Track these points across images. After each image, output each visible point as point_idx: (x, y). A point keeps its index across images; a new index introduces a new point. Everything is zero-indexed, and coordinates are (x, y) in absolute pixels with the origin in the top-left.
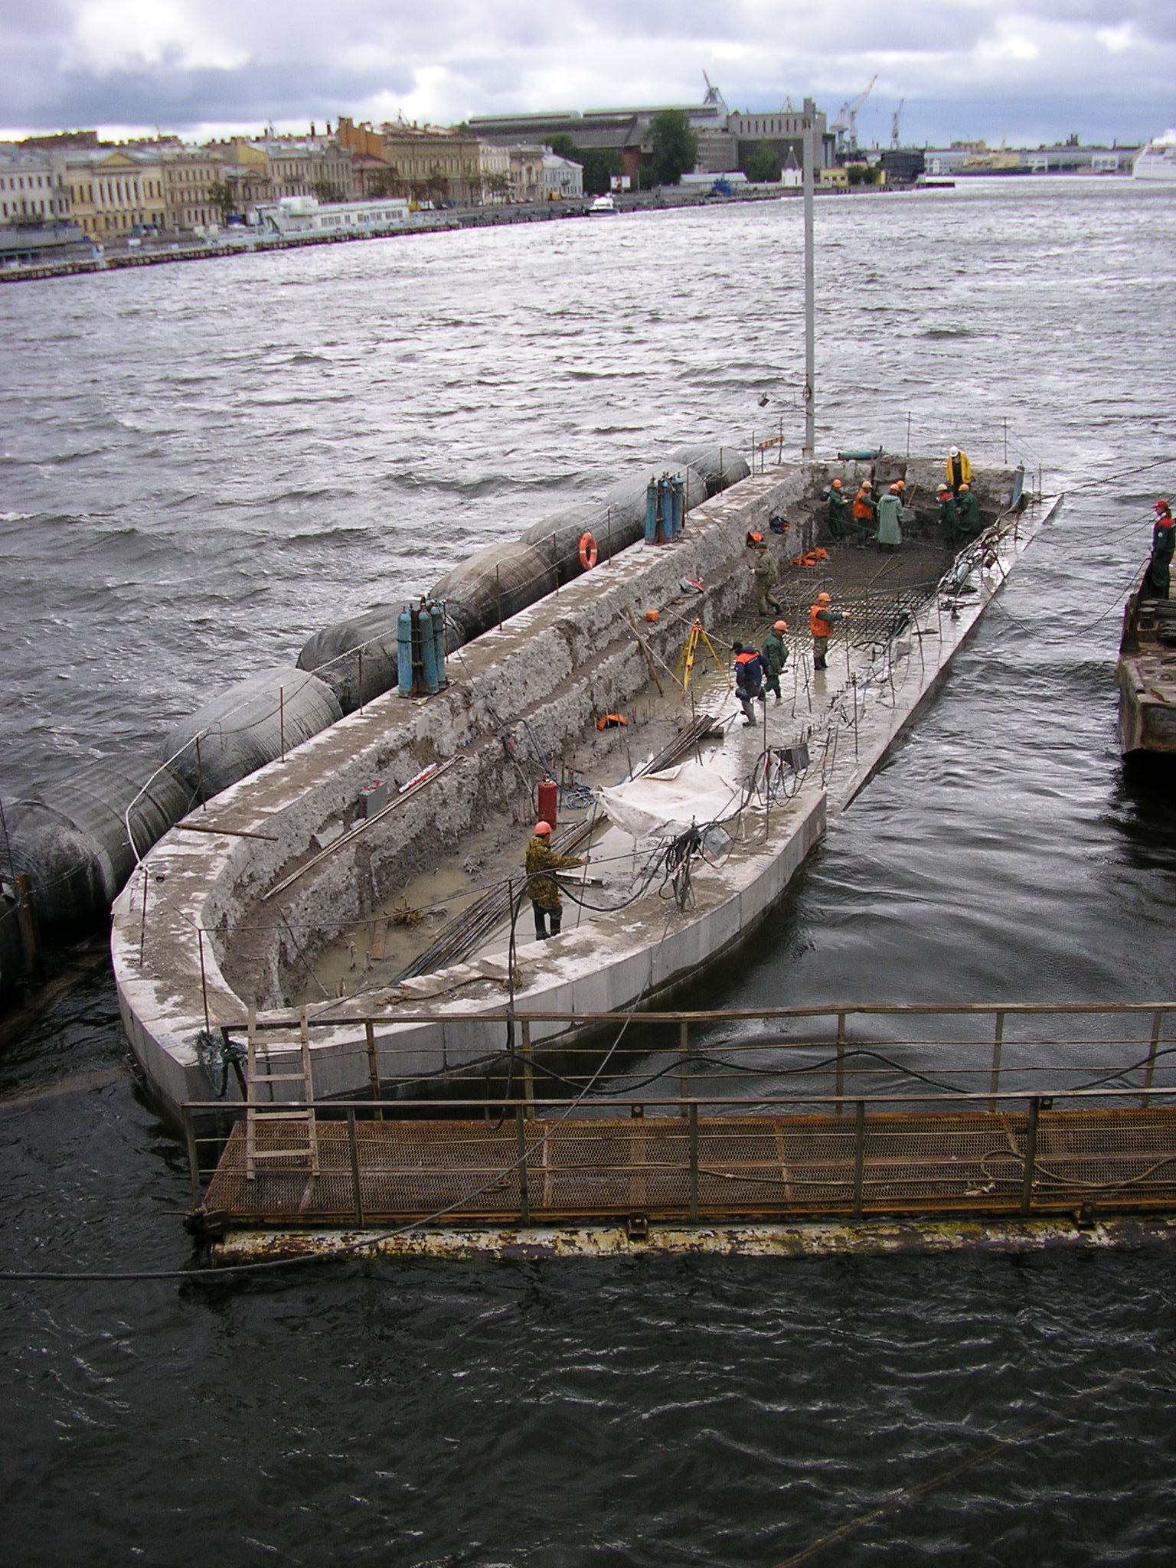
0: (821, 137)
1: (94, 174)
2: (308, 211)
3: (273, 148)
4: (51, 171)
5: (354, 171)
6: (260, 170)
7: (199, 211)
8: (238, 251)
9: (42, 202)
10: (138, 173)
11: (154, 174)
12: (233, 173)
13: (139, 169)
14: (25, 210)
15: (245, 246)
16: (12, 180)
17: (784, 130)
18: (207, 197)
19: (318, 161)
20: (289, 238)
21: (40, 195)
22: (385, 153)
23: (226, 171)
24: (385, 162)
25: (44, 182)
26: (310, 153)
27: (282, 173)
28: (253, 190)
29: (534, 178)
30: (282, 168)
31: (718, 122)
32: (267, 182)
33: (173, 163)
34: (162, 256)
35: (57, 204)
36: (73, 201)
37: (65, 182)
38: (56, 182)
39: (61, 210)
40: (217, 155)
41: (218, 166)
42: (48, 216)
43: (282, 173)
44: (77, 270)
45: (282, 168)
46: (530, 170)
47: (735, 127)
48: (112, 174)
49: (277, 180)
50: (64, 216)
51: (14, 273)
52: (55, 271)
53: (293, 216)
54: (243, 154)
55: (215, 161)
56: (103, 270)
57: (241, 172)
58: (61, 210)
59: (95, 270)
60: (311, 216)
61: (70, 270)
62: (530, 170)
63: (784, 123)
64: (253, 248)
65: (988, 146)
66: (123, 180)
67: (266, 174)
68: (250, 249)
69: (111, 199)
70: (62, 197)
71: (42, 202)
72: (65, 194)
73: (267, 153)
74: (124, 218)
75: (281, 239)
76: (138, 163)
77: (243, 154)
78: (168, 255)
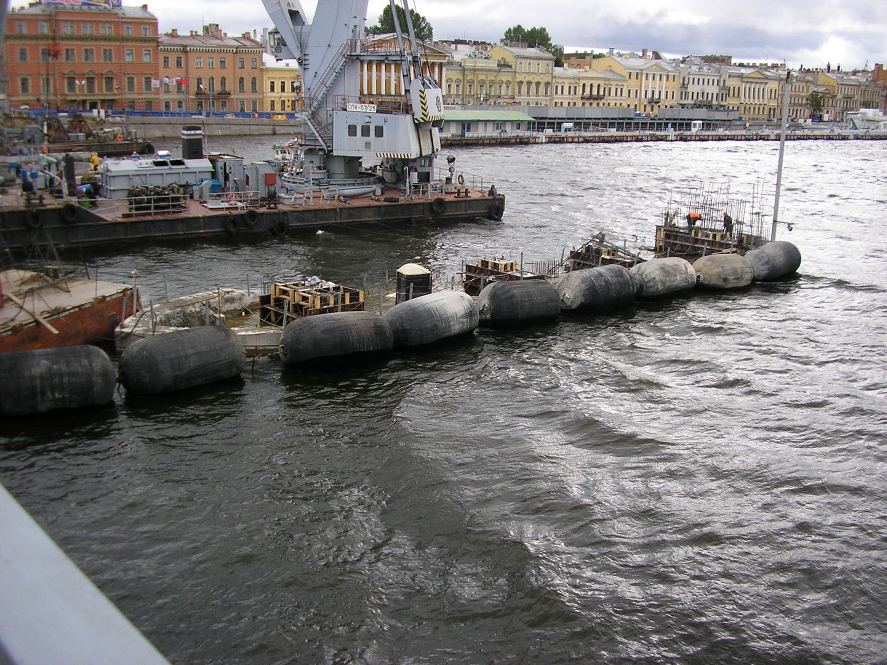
1: (742, 82)
2: (877, 118)
3: (839, 78)
4: (721, 77)
5: (882, 96)
6: (831, 89)
7: (795, 109)
8: (844, 138)
9: (693, 93)
10: (766, 83)
11: (774, 85)
12: (815, 89)
13: (767, 81)
15: (848, 136)
16: (699, 79)
18: (804, 102)
19: (863, 88)
20: (872, 134)
21: (713, 90)
23: (812, 88)
25: (716, 83)
26: (860, 83)
27: (843, 93)
28: (826, 100)
30: (843, 89)
32: (834, 97)
34: (595, 137)
35: (720, 96)
38: (722, 84)
39: (722, 100)
40: (809, 78)
42: (714, 102)
43: (843, 93)
44: (758, 138)
45: (843, 89)
48: (752, 82)
49: (839, 96)
50: (723, 103)
51: (612, 136)
52: (702, 137)
53: (868, 120)
54: (821, 79)
55: (808, 82)
56: (772, 140)
57: (821, 89)
58: (722, 100)
59: (768, 140)
60: (878, 122)
61: (755, 137)
64: (852, 138)
65: (126, 416)
66: (758, 86)
67: (834, 92)
68: (850, 138)
69: (749, 97)
70: (725, 92)
71: (693, 93)
72: (726, 92)
73: (836, 80)
74: (754, 108)
75: (868, 134)
76: (767, 78)
77: (821, 79)
78: (716, 135)
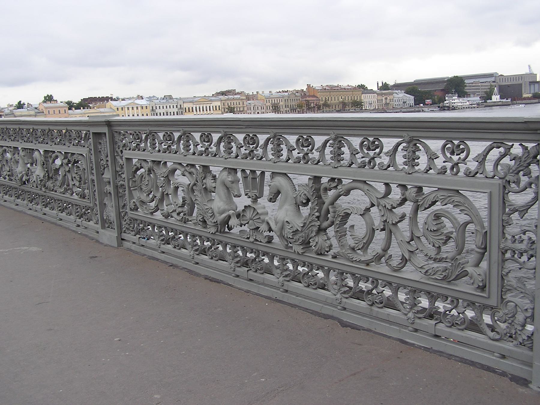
0: (528, 83)
14: (293, 107)
17: (515, 81)
22: (318, 95)
24: (318, 98)
25: (175, 107)
29: (388, 101)
31: (493, 79)
33: (225, 100)
36: (186, 112)
37: (182, 107)
38: (179, 107)
41: (243, 101)
43: (271, 102)
46: (386, 99)
47: (498, 81)
55: (242, 99)
62: (386, 99)
63: (515, 78)
70: (181, 111)
